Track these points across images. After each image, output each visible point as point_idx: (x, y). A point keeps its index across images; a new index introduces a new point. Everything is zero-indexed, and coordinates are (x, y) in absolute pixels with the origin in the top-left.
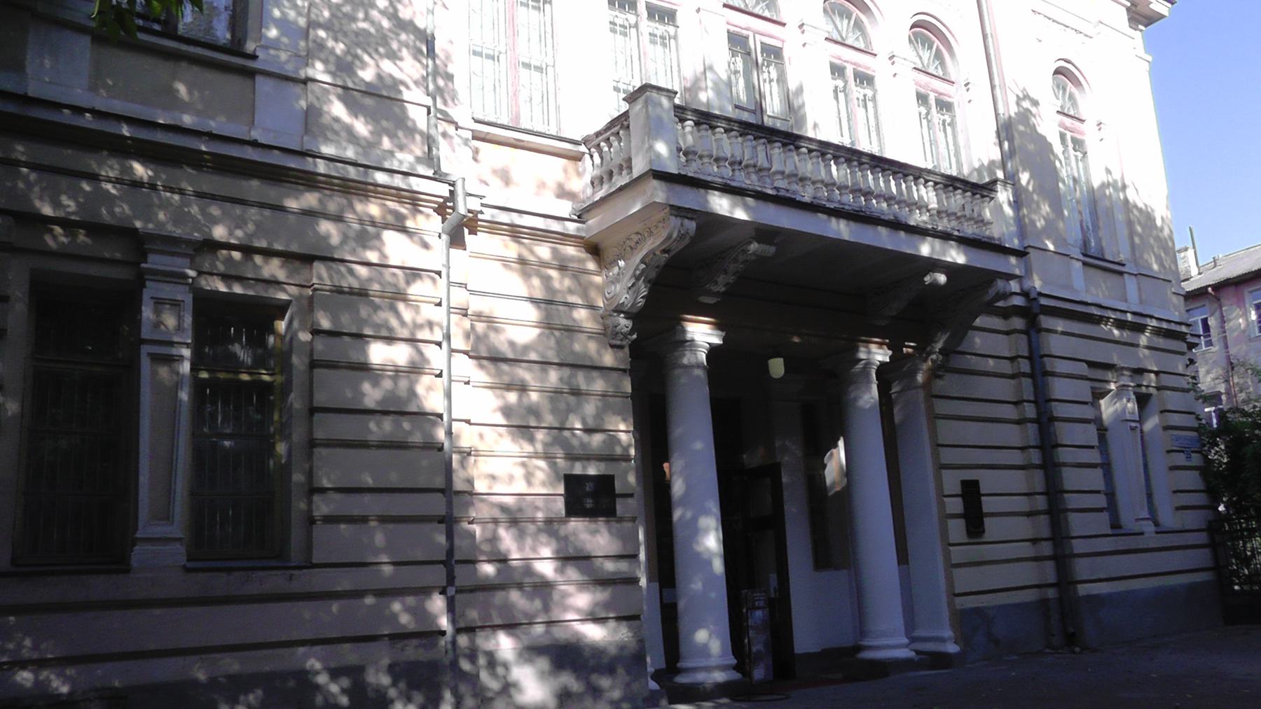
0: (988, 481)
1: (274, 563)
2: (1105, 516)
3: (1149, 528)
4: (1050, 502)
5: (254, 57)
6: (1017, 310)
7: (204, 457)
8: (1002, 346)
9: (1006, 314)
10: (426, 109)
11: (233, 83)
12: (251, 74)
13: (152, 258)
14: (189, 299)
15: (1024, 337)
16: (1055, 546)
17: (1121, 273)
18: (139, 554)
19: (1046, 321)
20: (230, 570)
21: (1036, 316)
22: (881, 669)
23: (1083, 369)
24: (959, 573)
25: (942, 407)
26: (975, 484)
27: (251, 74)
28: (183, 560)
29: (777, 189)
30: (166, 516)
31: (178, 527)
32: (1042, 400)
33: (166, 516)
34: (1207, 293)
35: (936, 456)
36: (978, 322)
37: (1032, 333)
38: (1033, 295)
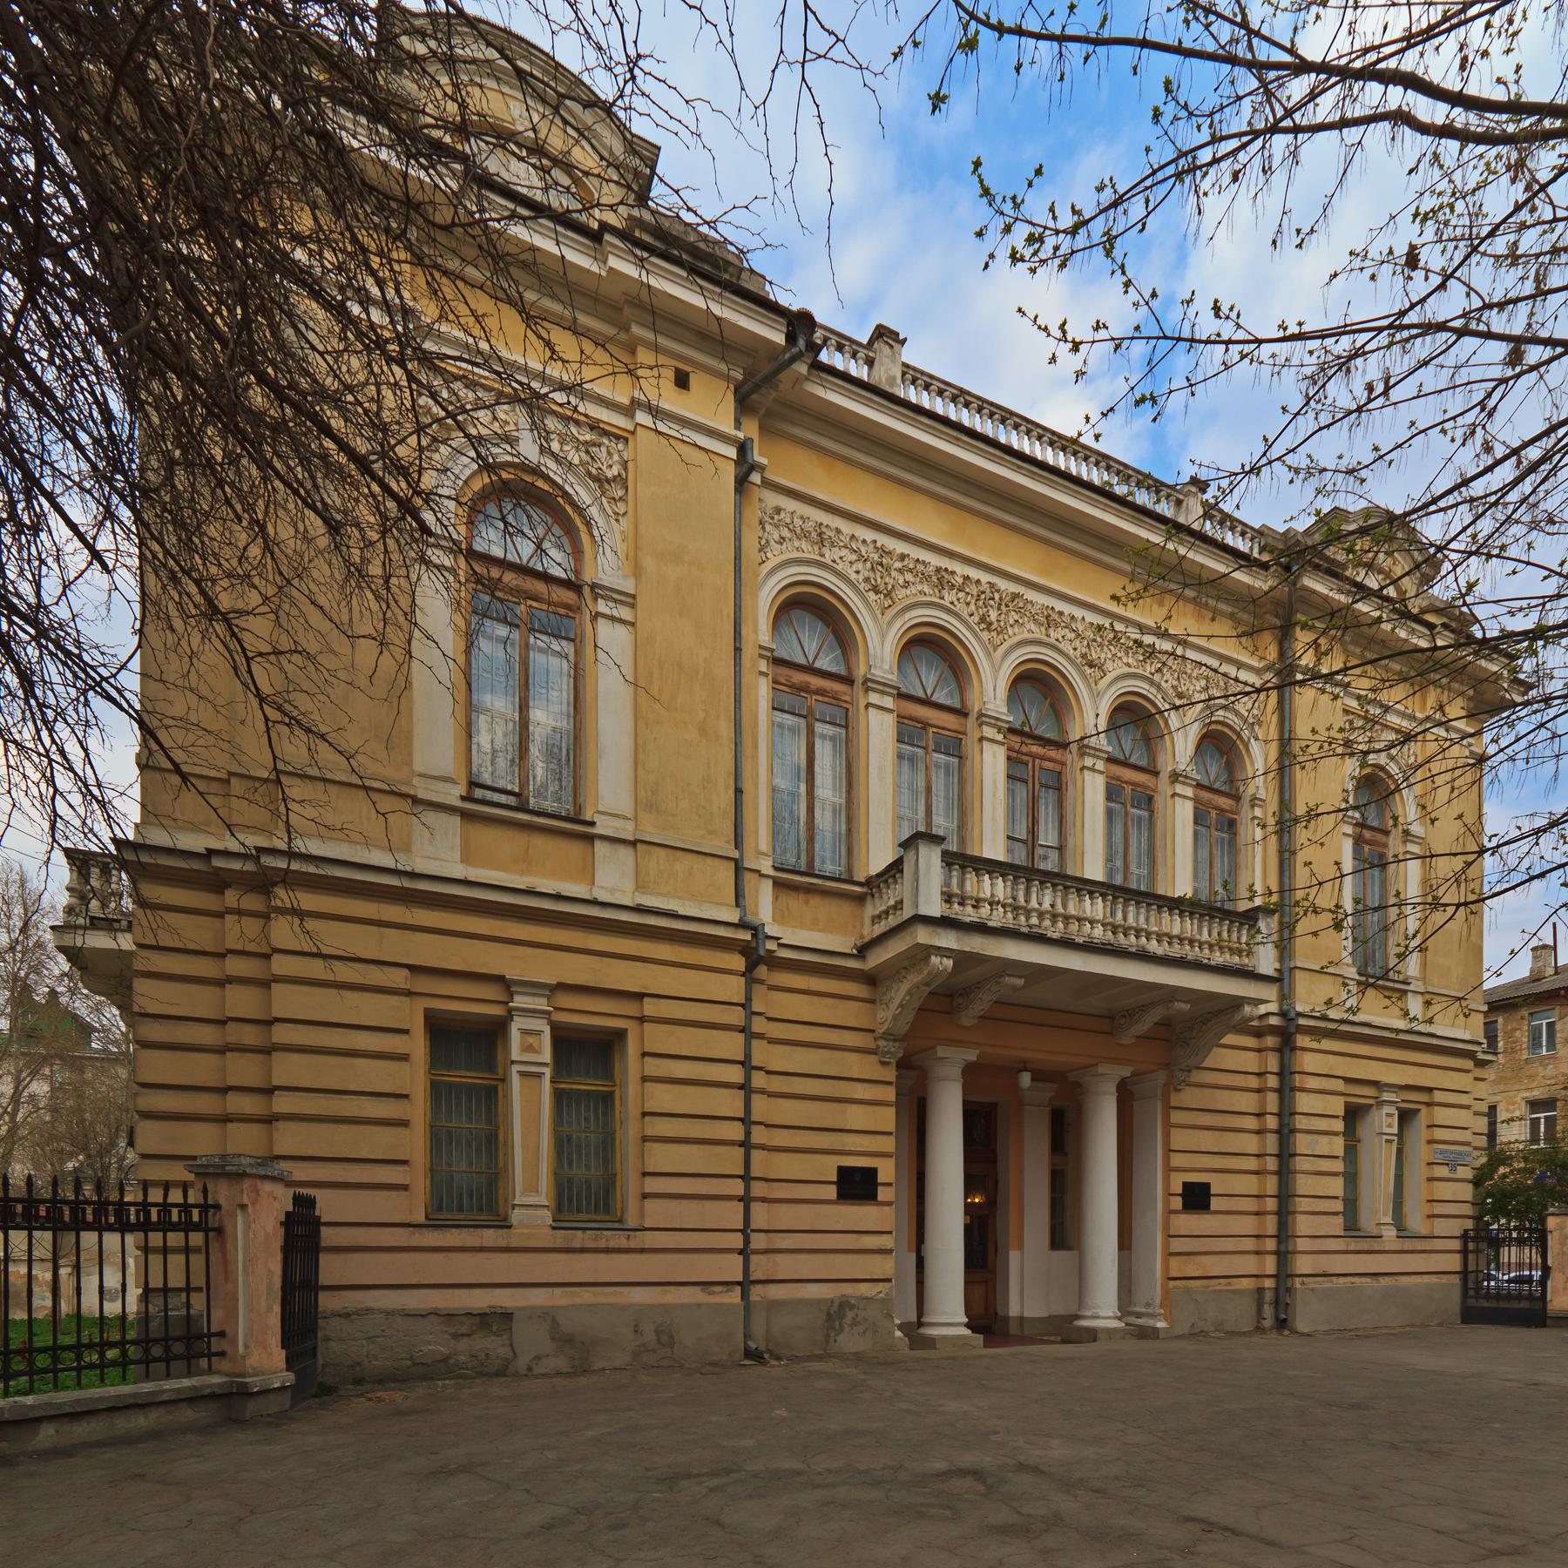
0: (328, 1205)
1: (617, 1225)
2: (1340, 1220)
3: (1390, 1233)
4: (1280, 1204)
5: (592, 824)
6: (1274, 1030)
7: (562, 1144)
8: (1250, 1061)
9: (1258, 1033)
10: (732, 865)
11: (574, 849)
12: (590, 839)
13: (517, 998)
14: (547, 1030)
15: (1277, 1055)
16: (1279, 1243)
17: (1405, 992)
18: (516, 1216)
19: (1302, 1041)
20: (584, 1229)
21: (1292, 1034)
22: (1092, 1335)
23: (1339, 1085)
24: (1174, 1261)
25: (1176, 1117)
26: (1205, 1187)
27: (590, 839)
28: (550, 1222)
29: (1030, 927)
30: (533, 1188)
31: (544, 1195)
32: (1286, 1112)
33: (533, 1188)
34: (1559, 996)
35: (1167, 1160)
36: (1225, 1041)
37: (1287, 1051)
38: (1292, 1015)
